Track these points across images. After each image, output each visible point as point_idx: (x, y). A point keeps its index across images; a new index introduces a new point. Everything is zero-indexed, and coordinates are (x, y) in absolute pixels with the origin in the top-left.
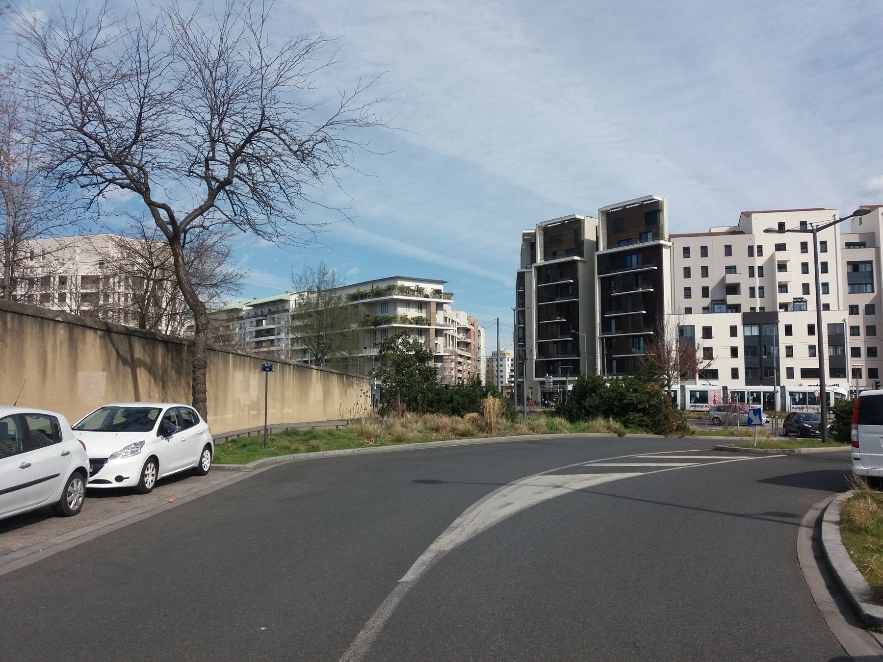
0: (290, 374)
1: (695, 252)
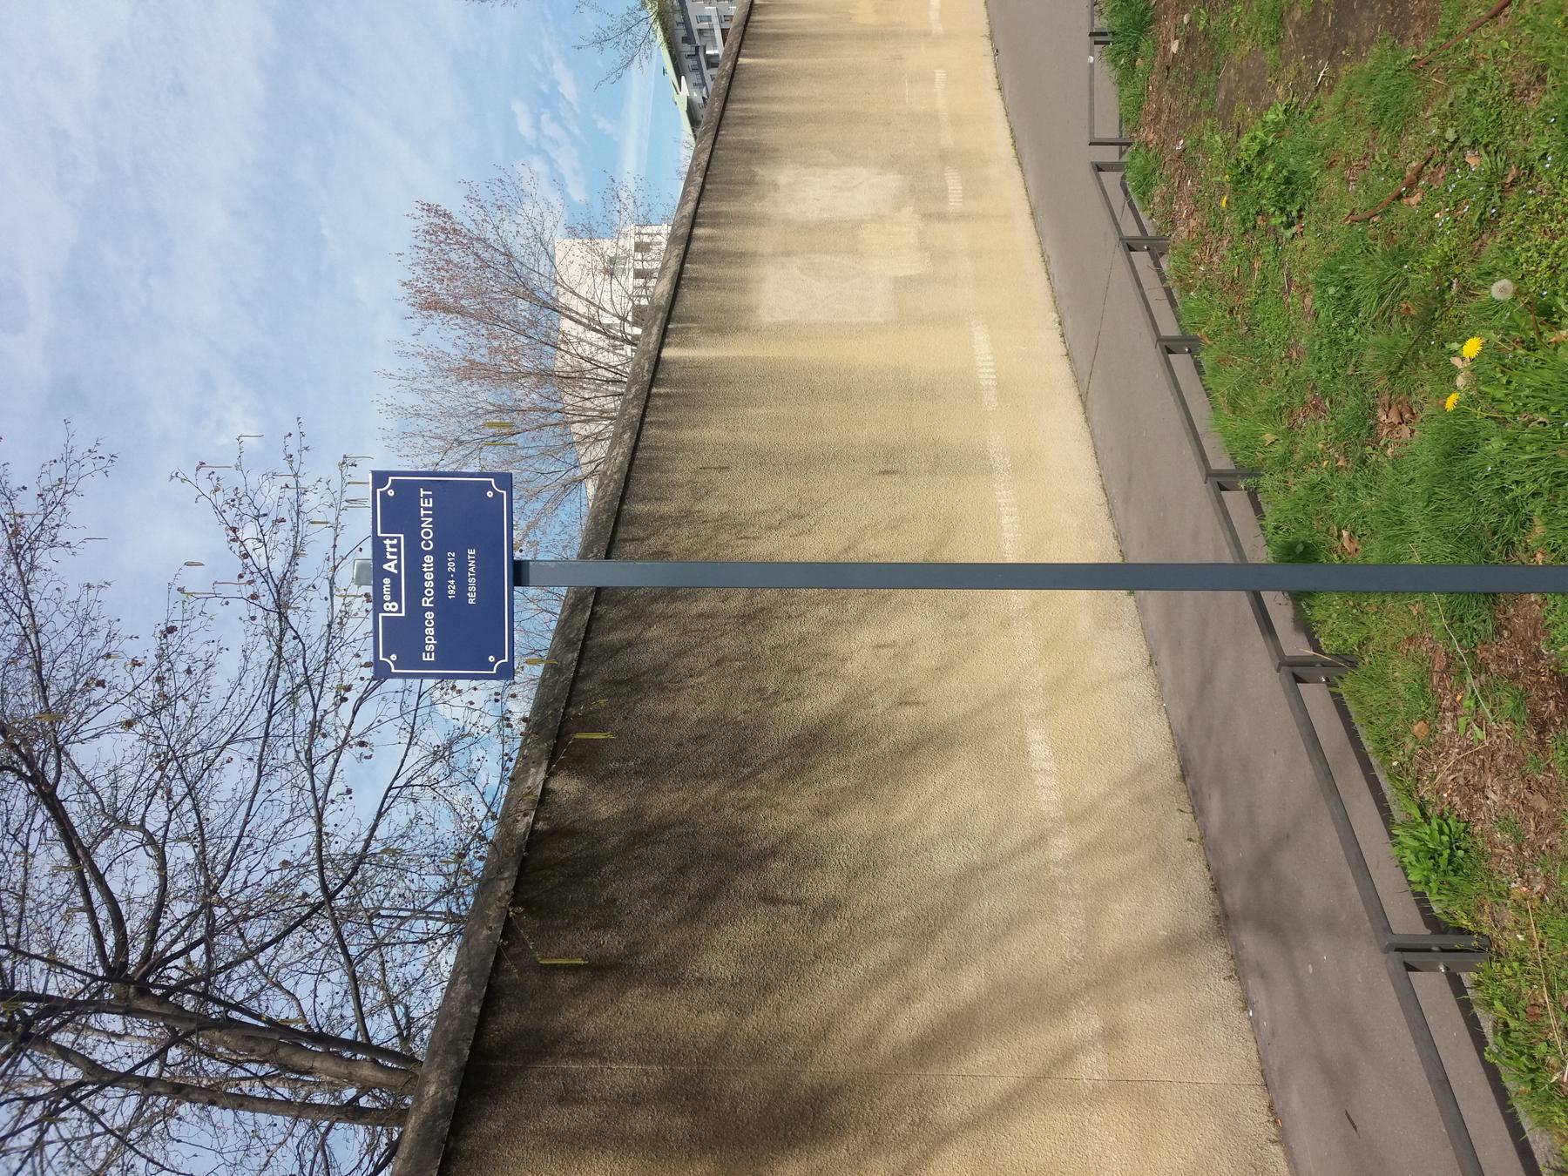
0: (757, 27)
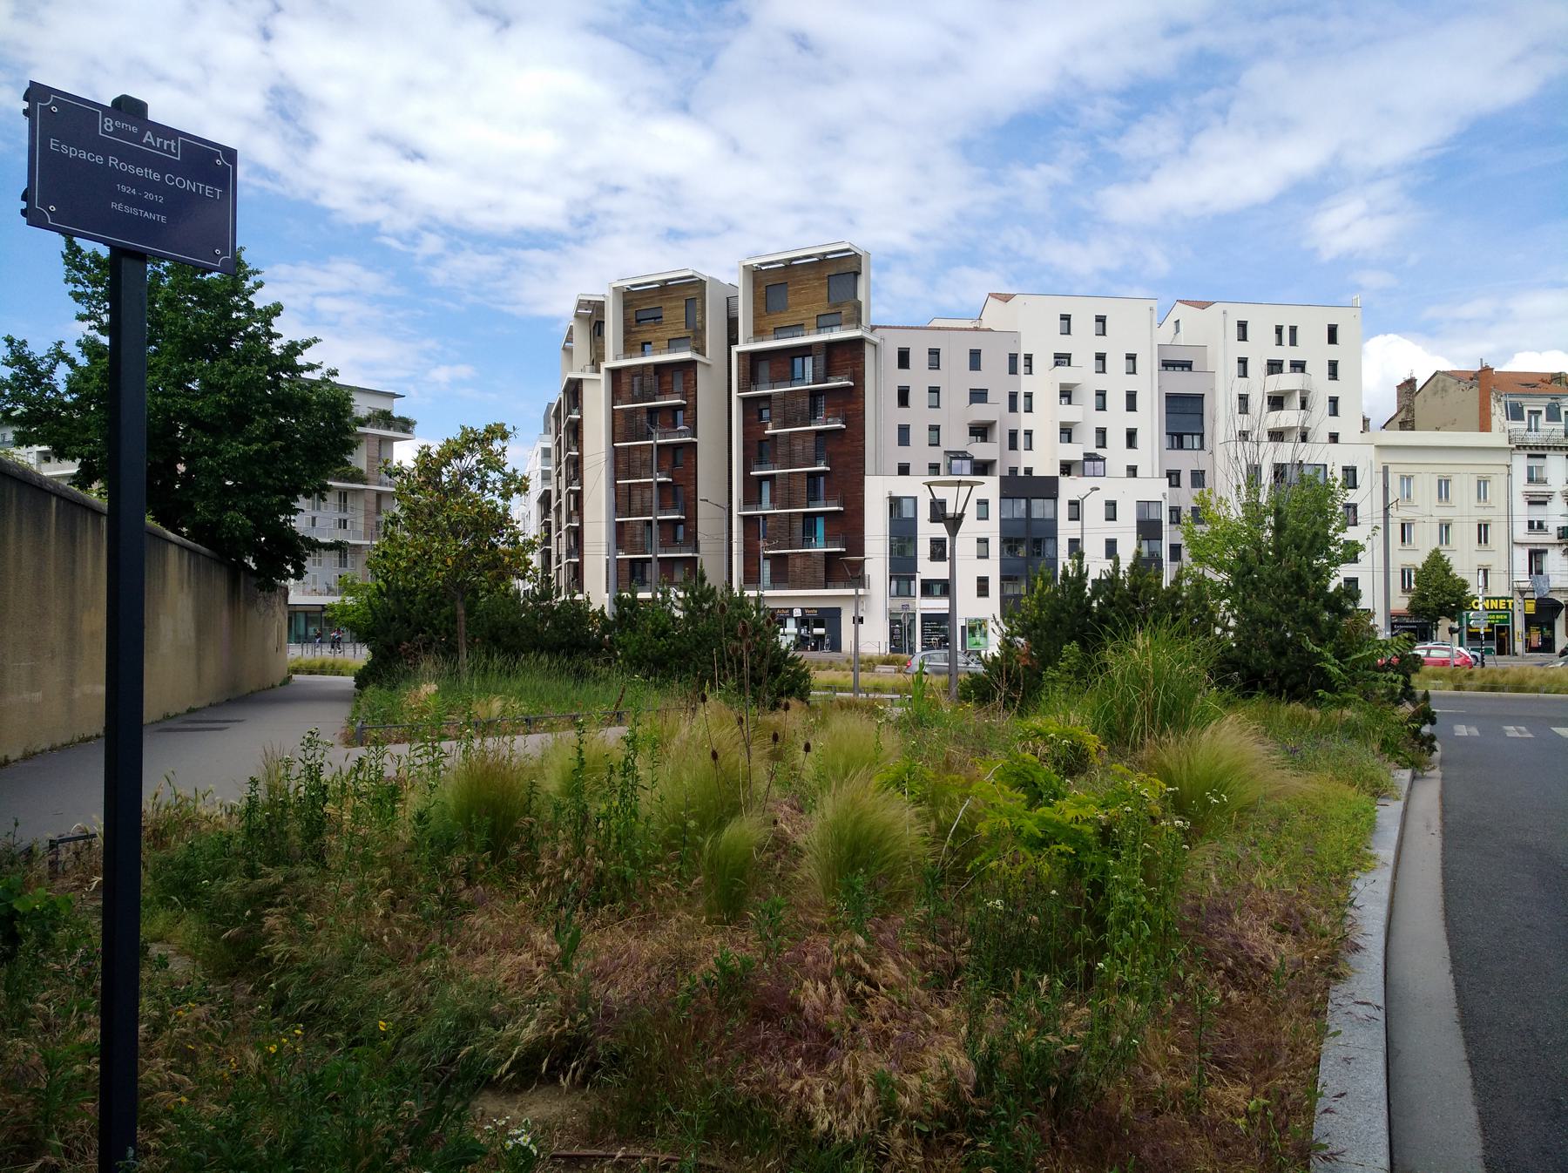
1: (919, 358)
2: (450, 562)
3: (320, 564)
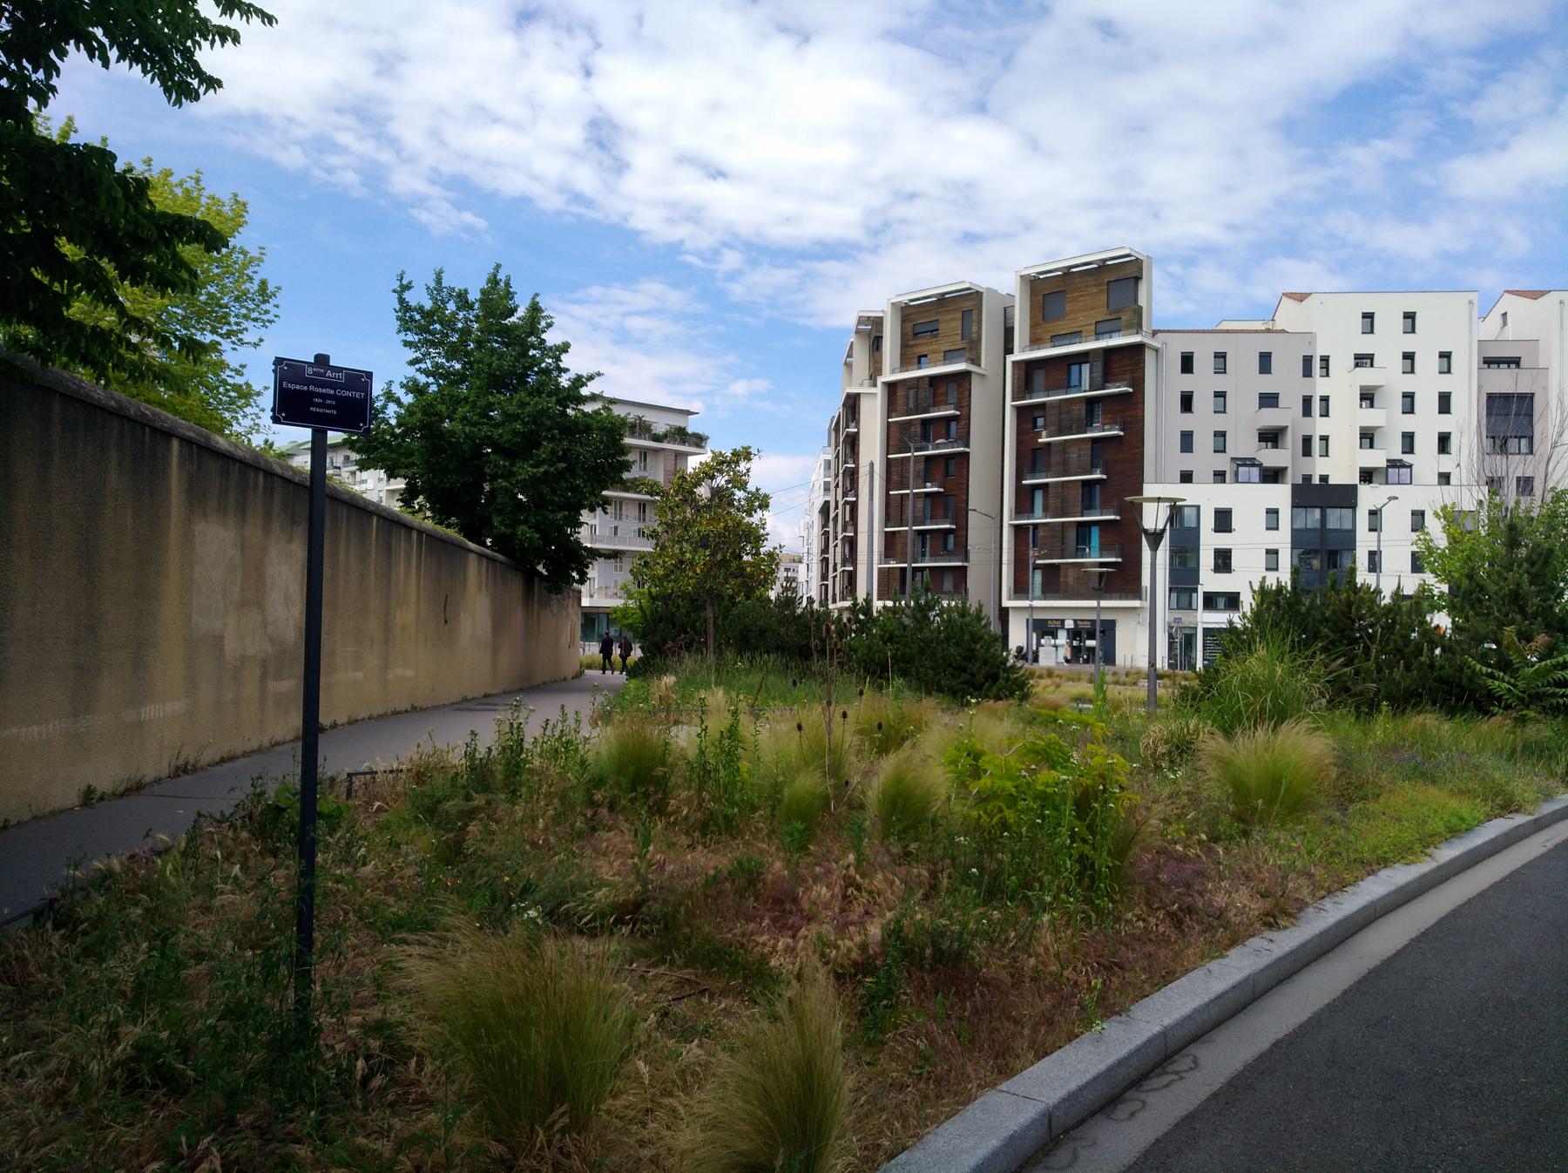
1: (1204, 363)
2: (698, 571)
3: (621, 570)
